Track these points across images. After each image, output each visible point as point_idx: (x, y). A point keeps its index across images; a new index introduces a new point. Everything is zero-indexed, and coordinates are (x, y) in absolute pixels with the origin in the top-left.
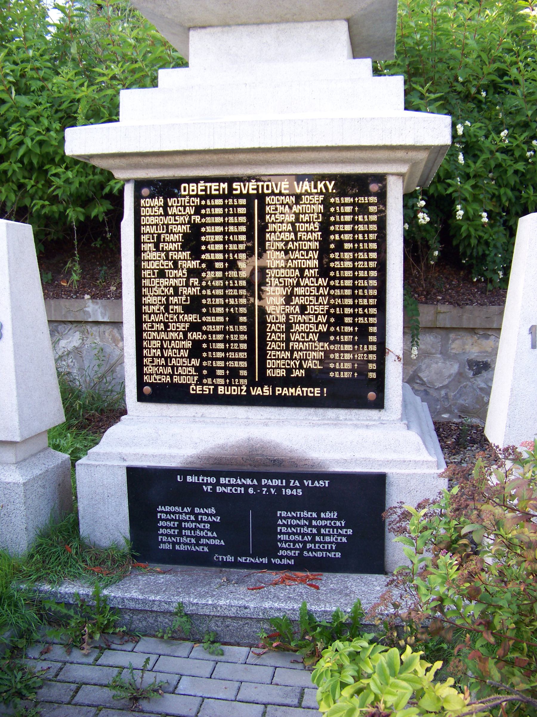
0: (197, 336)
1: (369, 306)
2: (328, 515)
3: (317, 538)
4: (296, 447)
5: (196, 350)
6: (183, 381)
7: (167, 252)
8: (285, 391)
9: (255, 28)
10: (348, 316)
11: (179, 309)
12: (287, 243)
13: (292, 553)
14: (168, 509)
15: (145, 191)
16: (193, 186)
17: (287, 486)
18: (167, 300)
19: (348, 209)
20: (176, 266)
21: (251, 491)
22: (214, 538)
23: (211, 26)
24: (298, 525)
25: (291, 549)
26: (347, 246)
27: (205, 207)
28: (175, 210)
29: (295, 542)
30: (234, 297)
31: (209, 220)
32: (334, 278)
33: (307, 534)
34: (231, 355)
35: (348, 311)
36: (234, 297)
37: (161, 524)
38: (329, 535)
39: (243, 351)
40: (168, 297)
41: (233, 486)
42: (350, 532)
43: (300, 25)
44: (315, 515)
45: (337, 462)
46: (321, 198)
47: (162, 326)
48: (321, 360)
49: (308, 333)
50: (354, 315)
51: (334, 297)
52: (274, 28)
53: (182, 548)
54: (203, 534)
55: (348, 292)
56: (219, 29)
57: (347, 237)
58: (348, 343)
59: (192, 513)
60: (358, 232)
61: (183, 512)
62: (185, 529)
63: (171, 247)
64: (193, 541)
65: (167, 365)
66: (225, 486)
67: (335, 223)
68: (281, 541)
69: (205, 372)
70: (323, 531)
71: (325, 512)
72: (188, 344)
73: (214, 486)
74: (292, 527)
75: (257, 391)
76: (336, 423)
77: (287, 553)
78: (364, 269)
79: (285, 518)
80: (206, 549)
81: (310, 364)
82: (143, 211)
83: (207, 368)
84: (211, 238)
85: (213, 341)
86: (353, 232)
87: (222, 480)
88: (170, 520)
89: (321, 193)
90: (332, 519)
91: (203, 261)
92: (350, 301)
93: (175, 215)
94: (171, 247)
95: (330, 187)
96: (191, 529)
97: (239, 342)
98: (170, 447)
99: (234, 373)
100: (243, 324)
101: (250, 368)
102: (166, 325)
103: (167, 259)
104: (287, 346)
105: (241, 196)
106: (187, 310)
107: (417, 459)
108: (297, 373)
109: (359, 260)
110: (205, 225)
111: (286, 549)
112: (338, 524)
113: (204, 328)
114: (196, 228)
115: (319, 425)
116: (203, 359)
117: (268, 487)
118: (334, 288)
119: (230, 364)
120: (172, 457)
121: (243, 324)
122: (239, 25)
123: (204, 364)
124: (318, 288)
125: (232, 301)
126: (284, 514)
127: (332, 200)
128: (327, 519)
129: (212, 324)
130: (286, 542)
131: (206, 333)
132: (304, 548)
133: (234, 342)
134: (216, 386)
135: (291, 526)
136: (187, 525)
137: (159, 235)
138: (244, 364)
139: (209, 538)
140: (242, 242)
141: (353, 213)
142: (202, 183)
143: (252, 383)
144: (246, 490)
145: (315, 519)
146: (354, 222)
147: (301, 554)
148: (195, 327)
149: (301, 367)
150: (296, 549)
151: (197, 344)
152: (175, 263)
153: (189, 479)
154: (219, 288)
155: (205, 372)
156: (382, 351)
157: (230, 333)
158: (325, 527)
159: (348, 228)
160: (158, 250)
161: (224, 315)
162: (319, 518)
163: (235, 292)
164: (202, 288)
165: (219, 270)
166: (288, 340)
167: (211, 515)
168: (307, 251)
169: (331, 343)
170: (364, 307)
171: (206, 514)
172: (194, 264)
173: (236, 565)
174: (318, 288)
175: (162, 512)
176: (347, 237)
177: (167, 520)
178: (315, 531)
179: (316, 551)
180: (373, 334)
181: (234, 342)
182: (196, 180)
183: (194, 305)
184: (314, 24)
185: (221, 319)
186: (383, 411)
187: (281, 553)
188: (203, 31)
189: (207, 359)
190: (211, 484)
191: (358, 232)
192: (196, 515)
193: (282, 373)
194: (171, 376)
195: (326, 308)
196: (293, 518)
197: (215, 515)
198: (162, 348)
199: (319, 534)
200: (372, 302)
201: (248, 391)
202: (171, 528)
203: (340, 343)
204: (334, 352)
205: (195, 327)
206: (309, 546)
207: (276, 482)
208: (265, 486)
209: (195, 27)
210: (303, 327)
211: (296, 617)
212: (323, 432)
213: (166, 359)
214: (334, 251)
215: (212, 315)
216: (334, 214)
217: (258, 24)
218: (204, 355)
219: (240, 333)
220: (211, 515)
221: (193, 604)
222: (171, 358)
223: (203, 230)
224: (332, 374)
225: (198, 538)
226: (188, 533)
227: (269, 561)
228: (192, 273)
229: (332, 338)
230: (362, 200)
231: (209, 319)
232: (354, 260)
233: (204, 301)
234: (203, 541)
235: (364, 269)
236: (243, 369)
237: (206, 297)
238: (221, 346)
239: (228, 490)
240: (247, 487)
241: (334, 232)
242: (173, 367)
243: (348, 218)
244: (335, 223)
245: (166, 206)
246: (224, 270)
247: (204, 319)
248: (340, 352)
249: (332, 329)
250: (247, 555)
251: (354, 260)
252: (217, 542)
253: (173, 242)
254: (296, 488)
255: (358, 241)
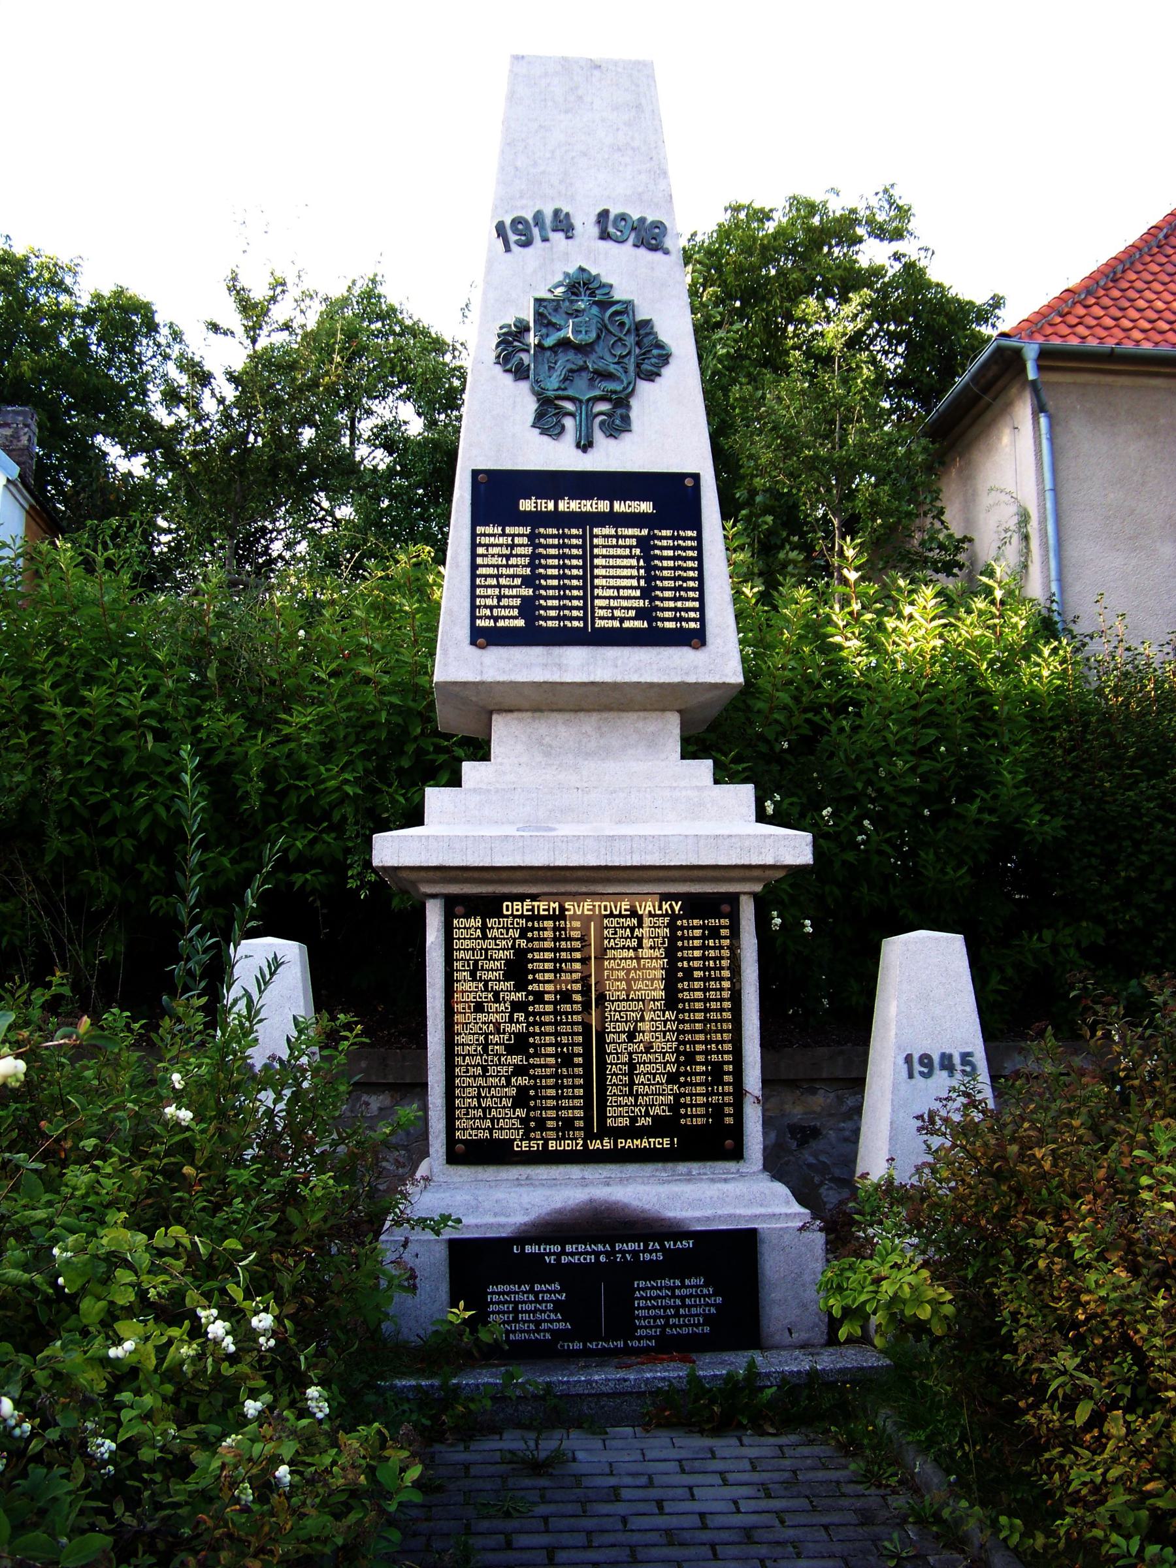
0: (523, 1081)
1: (723, 1042)
2: (694, 1281)
3: (682, 1311)
4: (647, 1207)
5: (521, 1099)
6: (504, 1136)
7: (486, 983)
8: (629, 1143)
9: (572, 715)
10: (700, 1053)
11: (501, 1049)
12: (629, 971)
13: (652, 1332)
14: (500, 1288)
15: (459, 910)
16: (517, 905)
17: (646, 1250)
18: (486, 1039)
19: (698, 933)
20: (497, 1000)
21: (602, 1258)
22: (558, 1321)
23: (519, 710)
24: (658, 1297)
25: (651, 1327)
26: (697, 974)
27: (533, 929)
28: (495, 933)
29: (655, 1318)
30: (567, 1034)
31: (536, 944)
32: (683, 1011)
33: (670, 1307)
34: (565, 1103)
35: (699, 1048)
36: (567, 1034)
37: (491, 1308)
38: (696, 1306)
39: (579, 1097)
40: (487, 1035)
41: (581, 1254)
42: (719, 1300)
43: (625, 715)
44: (678, 1283)
45: (698, 1220)
46: (667, 920)
47: (479, 1071)
48: (669, 1106)
49: (654, 1075)
50: (707, 1053)
51: (684, 1032)
52: (595, 717)
53: (518, 1336)
54: (544, 1316)
55: (699, 1026)
56: (529, 714)
57: (696, 964)
58: (701, 1084)
59: (532, 1291)
60: (709, 959)
61: (519, 1292)
62: (522, 1312)
63: (491, 975)
64: (532, 1326)
65: (485, 1118)
66: (572, 1254)
67: (683, 948)
68: (639, 1318)
69: (532, 1124)
70: (687, 1301)
71: (690, 1278)
72: (513, 1092)
73: (558, 1255)
74: (651, 1299)
75: (595, 1145)
76: (689, 1178)
77: (645, 1333)
78: (716, 1000)
79: (644, 1289)
80: (548, 1336)
81: (657, 1111)
82: (456, 933)
83: (535, 1119)
84: (540, 966)
85: (542, 1087)
86: (704, 958)
87: (568, 1248)
88: (503, 1303)
89: (667, 915)
90: (697, 1286)
91: (529, 993)
92: (702, 1037)
93: (495, 939)
94: (491, 975)
95: (677, 909)
96: (529, 1312)
97: (574, 1087)
98: (496, 1215)
99: (568, 1124)
100: (578, 1065)
101: (588, 1119)
102: (485, 1069)
103: (486, 990)
104: (631, 1090)
105: (574, 917)
106: (510, 1050)
107: (789, 1211)
108: (642, 1122)
109: (710, 990)
110: (532, 950)
111: (646, 1327)
112: (705, 1291)
113: (531, 1072)
114: (521, 953)
115: (669, 1182)
116: (530, 1109)
117: (623, 1252)
118: (683, 1021)
119: (563, 1114)
120: (503, 1226)
121: (578, 1065)
122: (553, 710)
123: (532, 1114)
124: (665, 1022)
125: (564, 1040)
126: (642, 1284)
127: (679, 923)
128: (691, 1287)
129: (541, 1066)
130: (645, 1318)
131: (534, 1077)
132: (667, 1324)
133: (568, 1087)
134: (546, 1141)
135: (651, 1298)
136: (525, 1307)
137: (476, 962)
138: (580, 1113)
139: (551, 1322)
140: (576, 971)
141: (703, 937)
142: (528, 902)
143: (589, 1136)
144: (597, 1258)
145: (679, 1288)
146: (704, 947)
147: (663, 1331)
148: (520, 1071)
149: (647, 1114)
150: (657, 1327)
151: (522, 1090)
152: (496, 994)
153: (528, 1249)
154: (550, 1023)
155: (532, 1124)
156: (739, 1092)
157: (562, 1077)
158: (691, 1296)
159: (697, 953)
160: (474, 979)
161: (556, 1056)
162: (683, 1286)
163: (569, 1029)
164: (529, 1024)
165: (549, 1003)
166: (631, 1083)
167: (554, 1292)
168: (652, 980)
169: (681, 1085)
170: (717, 1043)
171: (548, 1291)
172: (520, 996)
173: (586, 1353)
174: (665, 1022)
175: (493, 1293)
176: (696, 964)
177: (498, 1303)
178: (678, 1302)
179: (680, 1326)
180: (728, 1073)
181: (568, 1087)
182: (521, 898)
183: (519, 1045)
184: (642, 714)
185: (552, 1061)
186: (742, 1163)
187: (639, 1332)
188: (510, 716)
189: (535, 1108)
190: (554, 1253)
191: (709, 959)
192: (536, 1294)
193: (626, 1122)
194: (491, 1130)
195: (675, 1045)
196: (652, 1288)
197: (559, 1292)
198: (479, 1096)
199: (684, 1306)
200: (726, 1036)
201: (585, 1145)
202: (504, 1313)
203: (691, 1084)
204: (685, 1095)
205: (520, 1071)
206: (671, 1321)
207: (632, 1246)
208: (620, 1251)
209: (500, 711)
210: (649, 1068)
211: (684, 1385)
212: (676, 1188)
213: (484, 1110)
214: (682, 980)
215: (540, 1056)
216: (682, 938)
217: (576, 711)
218: (532, 1103)
219: (574, 1076)
220: (554, 1292)
221: (563, 1383)
222: (490, 1108)
223: (530, 956)
224: (683, 1121)
225: (538, 1323)
226: (526, 1317)
227: (626, 1344)
228: (517, 1006)
229: (682, 1079)
230: (713, 922)
231: (537, 1061)
232: (705, 990)
233: (531, 1040)
234: (544, 1326)
235: (716, 1000)
236: (579, 1118)
237: (534, 1034)
238: (552, 1092)
239: (575, 1259)
240: (597, 1254)
241: (682, 959)
242: (492, 1120)
243: (697, 943)
244: (683, 948)
245: (484, 928)
246: (555, 1003)
247: (531, 1061)
248: (691, 1095)
249: (682, 1069)
250: (599, 1338)
251: (705, 990)
252: (562, 1325)
253: (493, 971)
254: (656, 1251)
255: (709, 969)
